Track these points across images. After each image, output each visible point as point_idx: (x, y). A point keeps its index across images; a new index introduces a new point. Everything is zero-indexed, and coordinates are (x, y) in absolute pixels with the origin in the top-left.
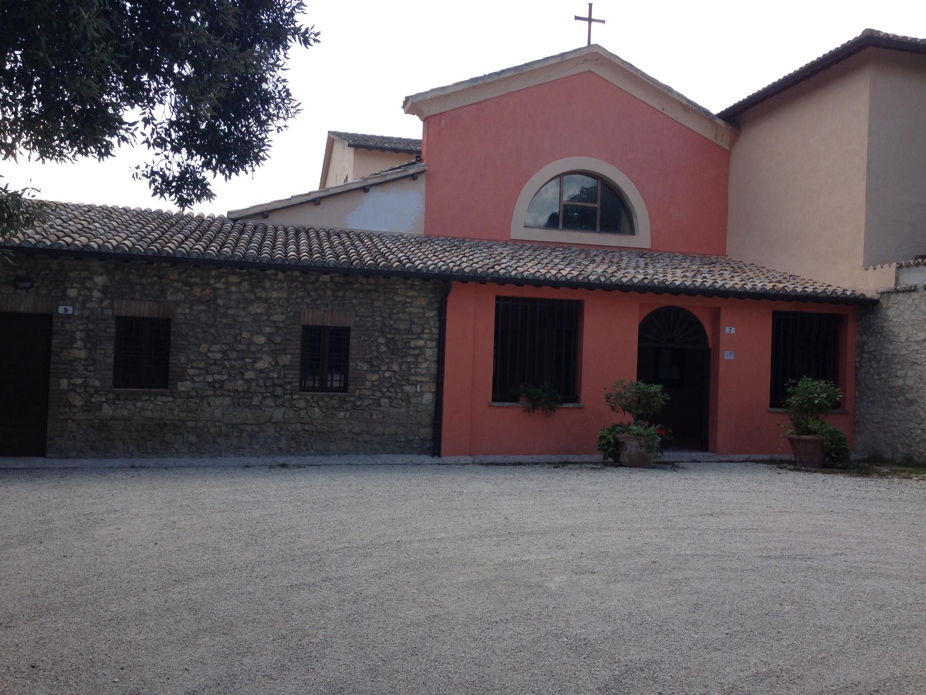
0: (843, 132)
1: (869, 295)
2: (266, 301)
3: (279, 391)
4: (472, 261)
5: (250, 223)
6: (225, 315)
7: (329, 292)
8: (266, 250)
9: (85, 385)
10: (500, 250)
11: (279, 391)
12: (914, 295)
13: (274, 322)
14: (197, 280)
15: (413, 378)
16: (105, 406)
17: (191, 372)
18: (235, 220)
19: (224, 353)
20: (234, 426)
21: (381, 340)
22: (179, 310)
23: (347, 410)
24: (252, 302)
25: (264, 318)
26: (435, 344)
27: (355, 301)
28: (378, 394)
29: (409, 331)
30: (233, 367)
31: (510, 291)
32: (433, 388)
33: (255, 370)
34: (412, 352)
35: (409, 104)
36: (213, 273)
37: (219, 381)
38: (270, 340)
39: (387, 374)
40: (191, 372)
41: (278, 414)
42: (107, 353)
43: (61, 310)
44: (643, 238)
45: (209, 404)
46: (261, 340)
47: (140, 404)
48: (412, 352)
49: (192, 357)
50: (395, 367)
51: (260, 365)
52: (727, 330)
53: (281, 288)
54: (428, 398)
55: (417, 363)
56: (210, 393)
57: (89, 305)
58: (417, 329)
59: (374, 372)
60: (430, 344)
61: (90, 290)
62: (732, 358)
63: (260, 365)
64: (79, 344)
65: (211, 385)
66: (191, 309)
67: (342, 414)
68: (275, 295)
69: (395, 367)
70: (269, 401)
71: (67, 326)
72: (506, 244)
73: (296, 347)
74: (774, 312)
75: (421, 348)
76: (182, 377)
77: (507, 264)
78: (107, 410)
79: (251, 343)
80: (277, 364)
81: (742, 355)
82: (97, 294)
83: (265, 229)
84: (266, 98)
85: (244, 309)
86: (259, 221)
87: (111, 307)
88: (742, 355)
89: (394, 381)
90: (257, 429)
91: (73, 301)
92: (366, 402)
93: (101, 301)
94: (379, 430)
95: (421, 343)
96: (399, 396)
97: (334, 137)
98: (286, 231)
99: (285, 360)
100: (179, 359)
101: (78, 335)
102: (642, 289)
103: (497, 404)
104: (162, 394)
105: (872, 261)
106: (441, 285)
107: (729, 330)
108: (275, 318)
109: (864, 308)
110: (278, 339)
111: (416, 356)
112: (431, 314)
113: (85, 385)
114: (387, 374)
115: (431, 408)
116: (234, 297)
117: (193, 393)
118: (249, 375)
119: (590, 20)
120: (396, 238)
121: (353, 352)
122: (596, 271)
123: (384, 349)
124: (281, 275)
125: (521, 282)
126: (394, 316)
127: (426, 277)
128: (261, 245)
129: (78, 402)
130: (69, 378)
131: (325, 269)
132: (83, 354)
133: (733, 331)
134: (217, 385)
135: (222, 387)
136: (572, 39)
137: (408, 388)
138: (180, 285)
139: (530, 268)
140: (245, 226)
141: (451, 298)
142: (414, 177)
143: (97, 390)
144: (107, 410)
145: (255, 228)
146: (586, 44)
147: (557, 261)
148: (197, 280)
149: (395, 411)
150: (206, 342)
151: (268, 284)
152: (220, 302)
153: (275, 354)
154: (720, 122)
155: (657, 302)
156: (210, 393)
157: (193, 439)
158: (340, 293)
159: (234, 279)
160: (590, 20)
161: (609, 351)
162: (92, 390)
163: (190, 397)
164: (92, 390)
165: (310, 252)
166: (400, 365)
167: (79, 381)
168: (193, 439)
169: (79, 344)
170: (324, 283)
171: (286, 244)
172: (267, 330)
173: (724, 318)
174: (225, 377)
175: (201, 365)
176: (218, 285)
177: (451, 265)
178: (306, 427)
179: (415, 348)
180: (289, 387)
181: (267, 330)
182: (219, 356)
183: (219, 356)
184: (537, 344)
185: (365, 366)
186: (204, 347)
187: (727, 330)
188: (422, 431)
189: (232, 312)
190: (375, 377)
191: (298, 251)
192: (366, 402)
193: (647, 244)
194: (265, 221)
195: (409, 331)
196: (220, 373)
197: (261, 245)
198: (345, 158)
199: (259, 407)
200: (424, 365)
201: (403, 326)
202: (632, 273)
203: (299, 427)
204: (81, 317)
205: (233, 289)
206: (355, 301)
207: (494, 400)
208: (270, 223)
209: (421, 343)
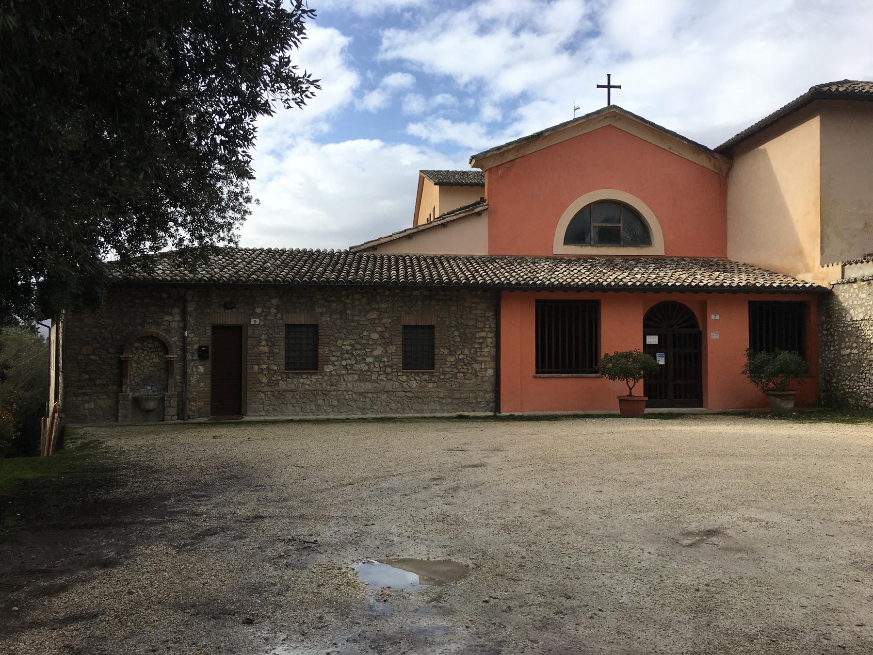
0: (796, 165)
1: (825, 284)
2: (378, 310)
3: (389, 370)
4: (520, 274)
5: (365, 255)
6: (353, 321)
7: (419, 302)
8: (377, 275)
9: (268, 369)
10: (543, 264)
11: (389, 370)
12: (855, 285)
13: (384, 324)
14: (333, 298)
15: (479, 359)
16: (281, 382)
17: (333, 359)
18: (355, 253)
19: (352, 346)
20: (360, 394)
21: (456, 334)
22: (323, 319)
23: (434, 382)
24: (367, 312)
25: (377, 321)
26: (493, 335)
27: (437, 308)
28: (455, 370)
29: (475, 326)
30: (358, 355)
31: (545, 296)
32: (493, 364)
33: (373, 356)
34: (477, 341)
35: (474, 161)
36: (344, 293)
37: (350, 365)
38: (382, 337)
39: (461, 357)
40: (333, 359)
41: (389, 386)
42: (280, 349)
43: (252, 322)
44: (658, 248)
45: (344, 380)
46: (375, 336)
47: (302, 380)
48: (477, 341)
49: (332, 349)
50: (466, 352)
51: (376, 353)
52: (713, 317)
53: (387, 301)
54: (490, 372)
55: (481, 348)
56: (344, 372)
57: (269, 318)
58: (480, 325)
59: (452, 355)
60: (490, 335)
61: (269, 308)
62: (717, 337)
63: (376, 353)
64: (264, 343)
65: (345, 367)
66: (331, 317)
67: (431, 385)
68: (383, 306)
69: (466, 352)
70: (382, 377)
71: (256, 332)
72: (547, 258)
73: (399, 341)
74: (750, 302)
75: (485, 338)
76: (327, 362)
77: (544, 275)
78: (282, 385)
79: (369, 338)
80: (387, 352)
81: (726, 339)
82: (273, 310)
83: (375, 258)
84: (348, 8)
85: (365, 316)
86: (370, 253)
87: (282, 319)
88: (726, 339)
89: (466, 361)
90: (375, 396)
91: (259, 316)
92: (447, 377)
93: (275, 315)
94: (457, 395)
95: (483, 334)
96: (470, 371)
97: (423, 175)
98: (389, 260)
99: (392, 349)
100: (323, 351)
101: (263, 337)
102: (644, 289)
103: (539, 375)
104: (315, 374)
105: (825, 262)
106: (495, 295)
107: (714, 317)
108: (384, 321)
109: (823, 297)
110: (387, 335)
111: (481, 343)
112: (490, 314)
113: (268, 369)
114: (461, 357)
115: (492, 379)
116: (357, 308)
117: (334, 373)
118: (369, 360)
119: (609, 87)
120: (469, 259)
121: (437, 342)
122: (610, 277)
123: (458, 339)
124: (387, 293)
125: (552, 288)
126: (465, 317)
127: (486, 288)
128: (373, 272)
129: (265, 380)
130: (259, 365)
131: (415, 286)
132: (266, 349)
133: (718, 317)
134: (349, 367)
135: (352, 369)
136: (596, 102)
137: (475, 366)
138: (323, 302)
139: (562, 275)
140: (361, 257)
141: (502, 303)
142: (479, 214)
143: (275, 372)
144: (282, 385)
145: (369, 257)
146: (606, 105)
147: (583, 271)
148: (333, 298)
149: (467, 381)
150: (341, 338)
151: (379, 299)
152: (349, 312)
153: (385, 345)
154: (717, 156)
155: (663, 297)
156: (344, 372)
157: (335, 403)
158: (427, 303)
159: (357, 296)
160: (609, 87)
161: (622, 334)
162: (272, 372)
163: (331, 375)
164: (272, 372)
165: (406, 276)
166: (470, 350)
167: (265, 367)
168: (335, 403)
169: (264, 343)
170: (416, 296)
171: (389, 270)
172: (380, 329)
173: (709, 309)
174: (354, 362)
175: (339, 354)
176: (347, 301)
177: (503, 279)
178: (408, 394)
179: (480, 338)
180: (395, 367)
181: (380, 329)
182: (349, 348)
183: (349, 348)
184: (567, 331)
185: (446, 352)
186: (340, 342)
187: (713, 317)
188: (487, 395)
189: (356, 318)
190: (452, 359)
191: (398, 276)
192: (447, 377)
193: (662, 253)
194: (375, 253)
195: (475, 326)
196: (350, 359)
197: (373, 272)
198: (433, 191)
199: (376, 381)
200: (486, 350)
201: (471, 323)
202: (637, 276)
203: (403, 394)
204: (264, 326)
205: (357, 303)
206: (437, 308)
207: (537, 372)
208: (378, 253)
209: (483, 334)
